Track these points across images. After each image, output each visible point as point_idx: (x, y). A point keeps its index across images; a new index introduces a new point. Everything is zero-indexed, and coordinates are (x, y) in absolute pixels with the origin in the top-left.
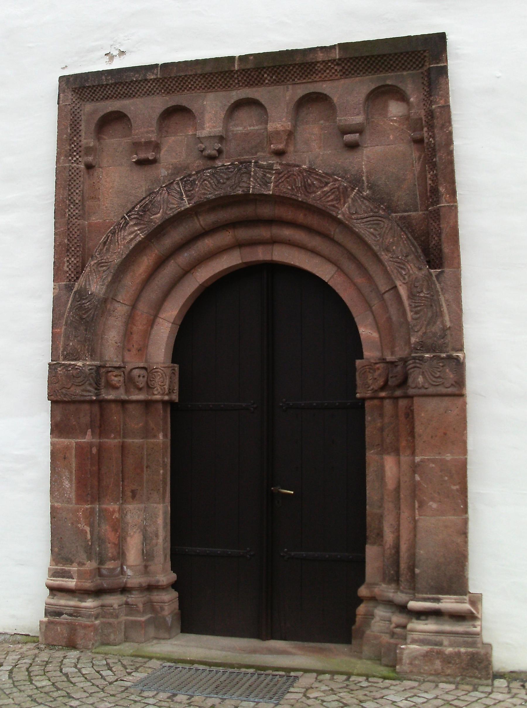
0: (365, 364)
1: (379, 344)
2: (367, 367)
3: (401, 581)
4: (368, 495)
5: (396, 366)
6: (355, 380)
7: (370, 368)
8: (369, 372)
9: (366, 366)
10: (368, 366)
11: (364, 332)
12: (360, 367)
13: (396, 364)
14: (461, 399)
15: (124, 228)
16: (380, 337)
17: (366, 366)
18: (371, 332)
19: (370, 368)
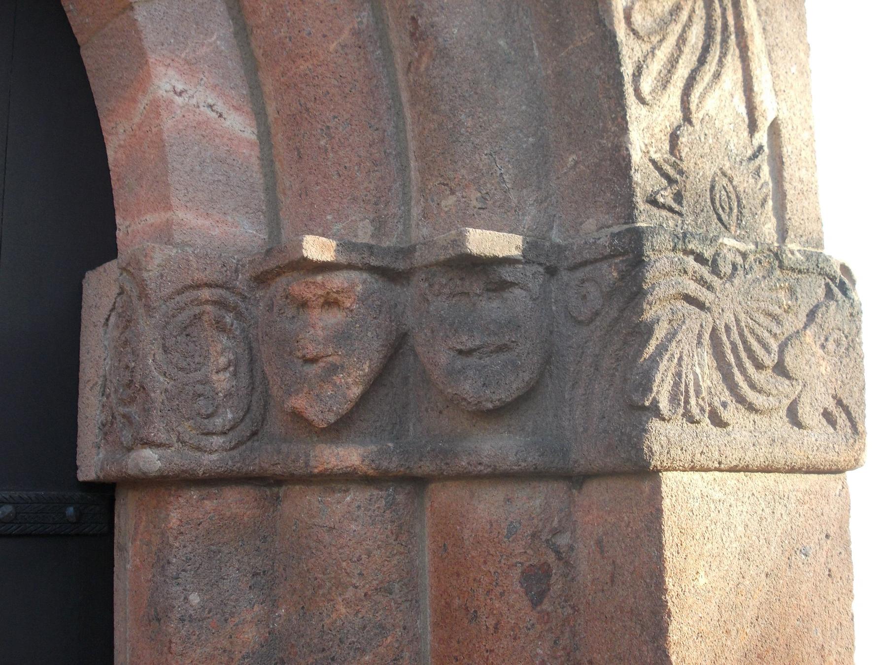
0: (199, 276)
1: (257, 176)
2: (205, 294)
3: (70, 11)
4: (115, 586)
5: (503, 286)
6: (114, 521)
7: (220, 304)
8: (220, 327)
9: (198, 286)
10: (209, 285)
11: (180, 94)
12: (167, 291)
13: (507, 273)
14: (646, 486)
15: (202, 384)
16: (265, 136)
17: (198, 286)
18: (220, 106)
19: (220, 304)
